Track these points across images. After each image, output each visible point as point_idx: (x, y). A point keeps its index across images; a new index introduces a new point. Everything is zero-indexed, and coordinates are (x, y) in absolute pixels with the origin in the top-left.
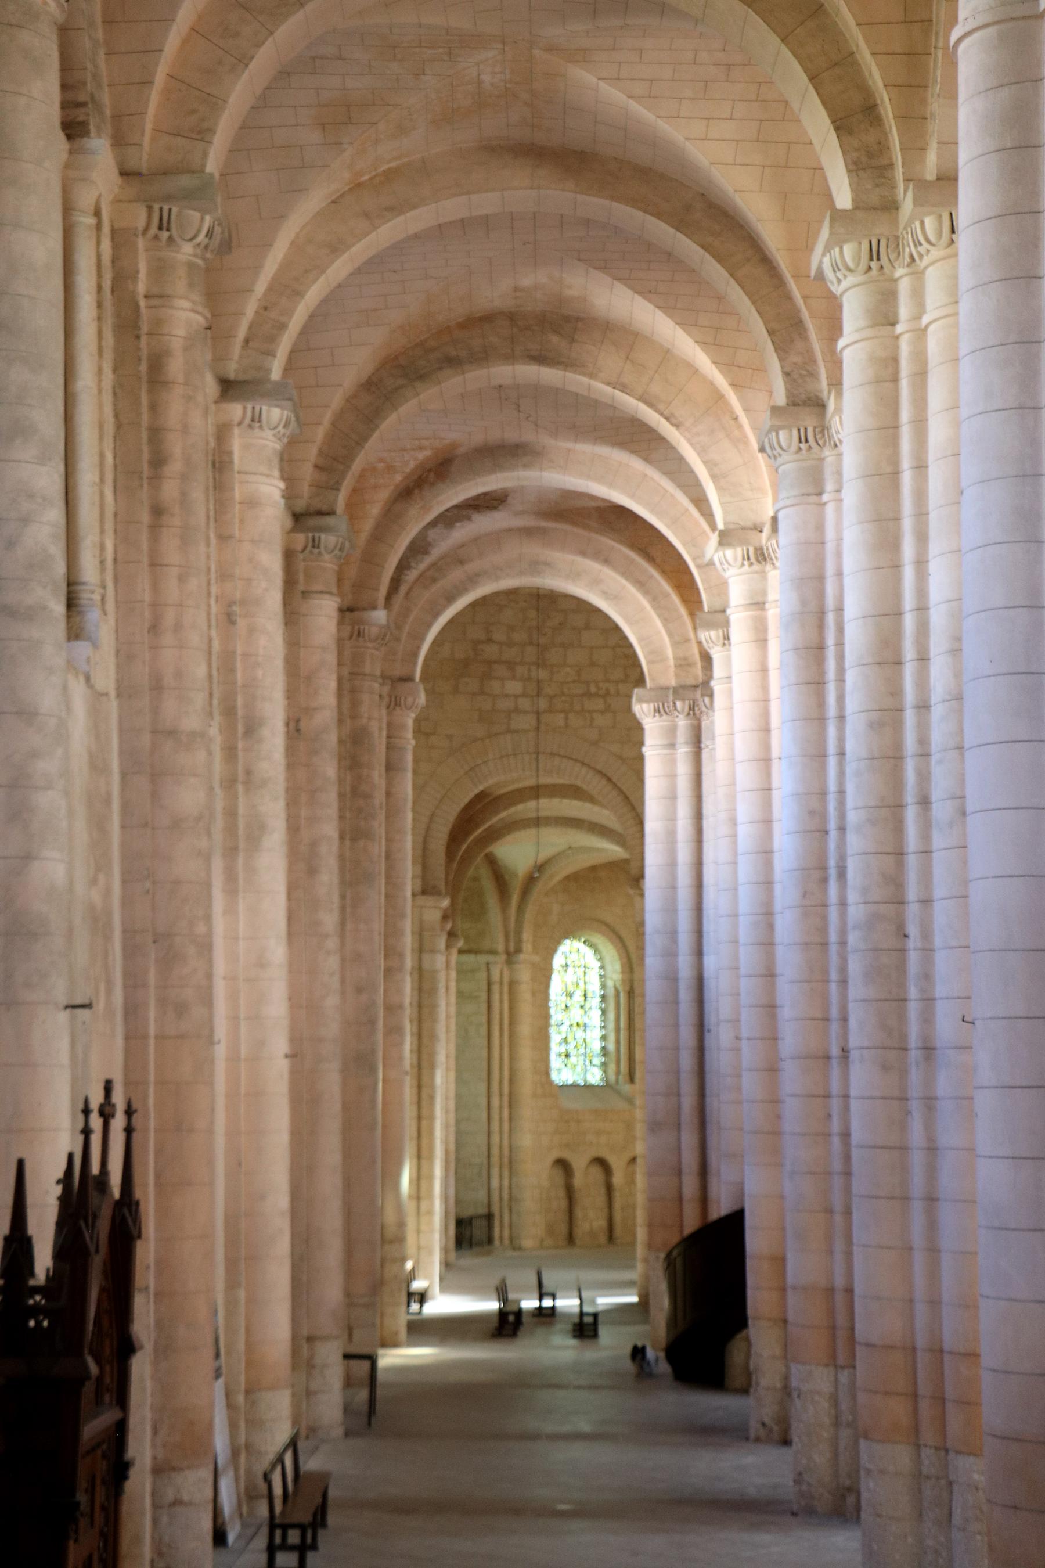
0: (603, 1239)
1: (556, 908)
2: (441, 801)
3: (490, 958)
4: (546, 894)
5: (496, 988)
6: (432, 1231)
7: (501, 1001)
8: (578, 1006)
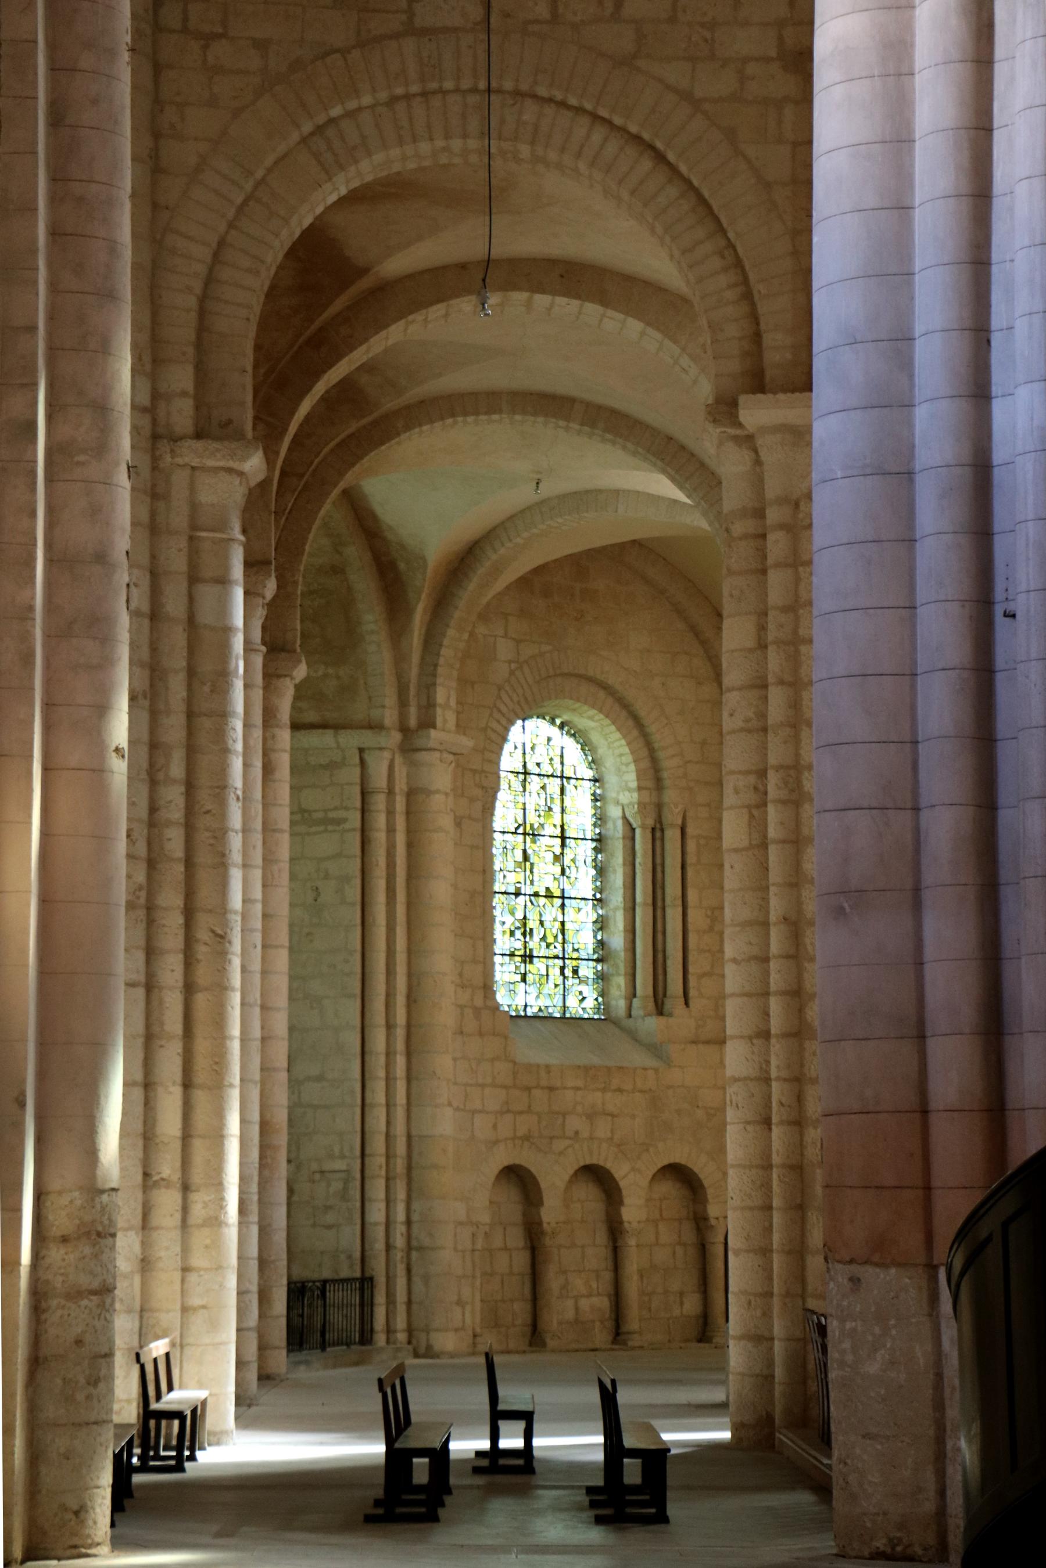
0: (601, 1336)
1: (504, 649)
2: (240, 209)
3: (366, 738)
4: (483, 617)
5: (379, 802)
6: (219, 1268)
7: (391, 830)
8: (550, 857)
